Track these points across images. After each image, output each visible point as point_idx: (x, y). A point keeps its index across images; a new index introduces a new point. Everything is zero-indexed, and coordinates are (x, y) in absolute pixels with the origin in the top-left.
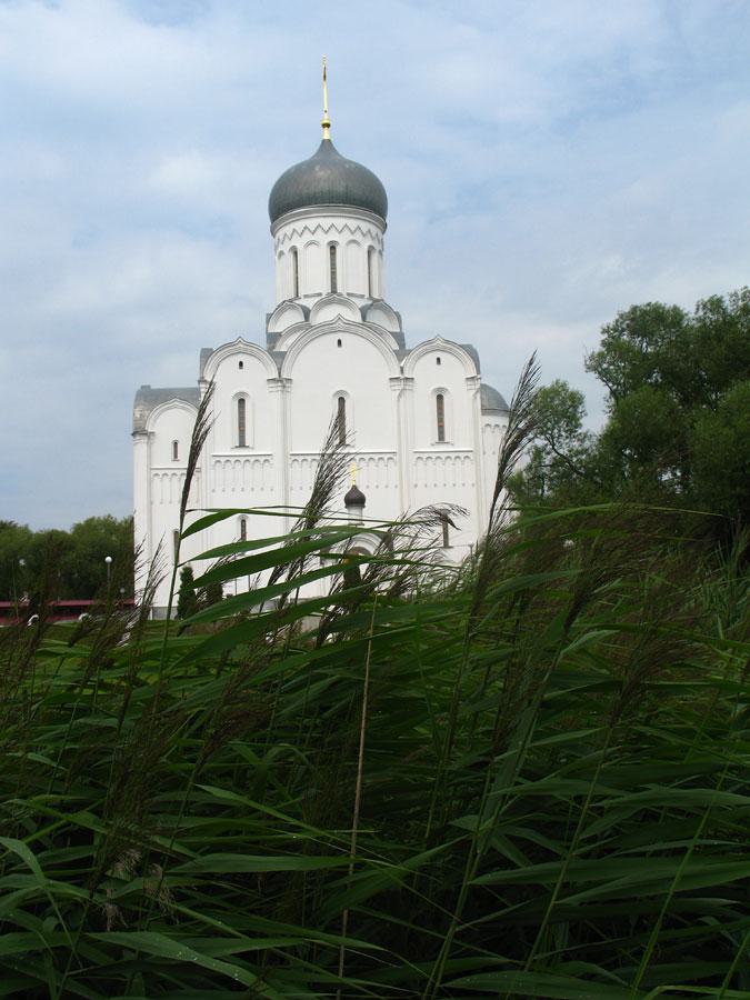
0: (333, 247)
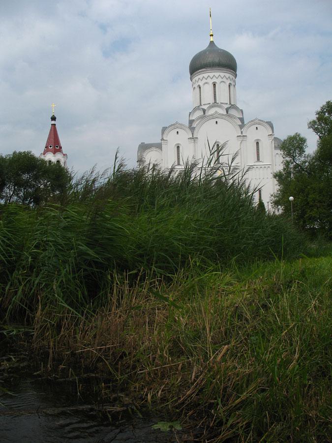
0: (214, 85)
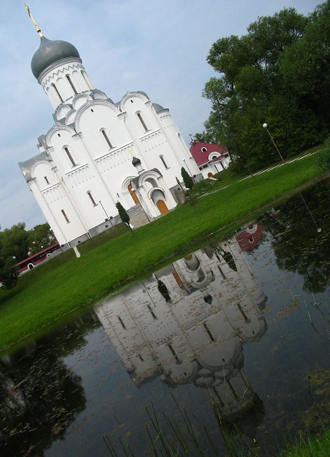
0: (68, 77)
